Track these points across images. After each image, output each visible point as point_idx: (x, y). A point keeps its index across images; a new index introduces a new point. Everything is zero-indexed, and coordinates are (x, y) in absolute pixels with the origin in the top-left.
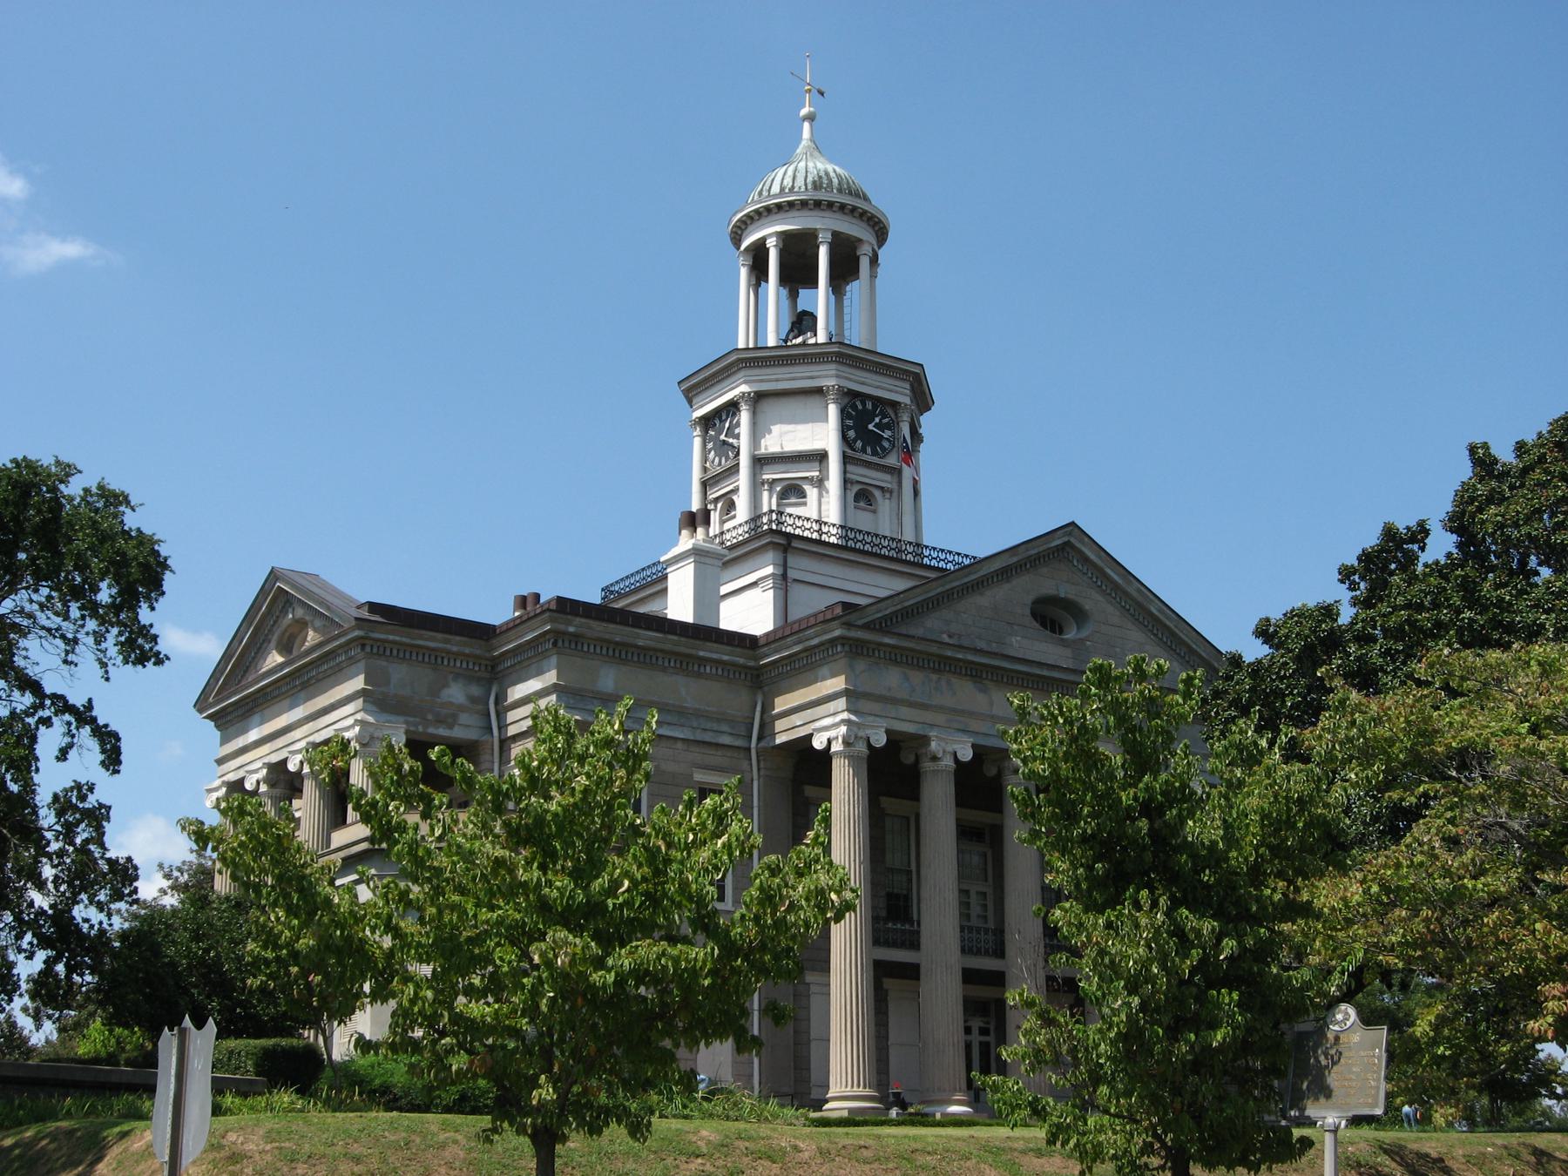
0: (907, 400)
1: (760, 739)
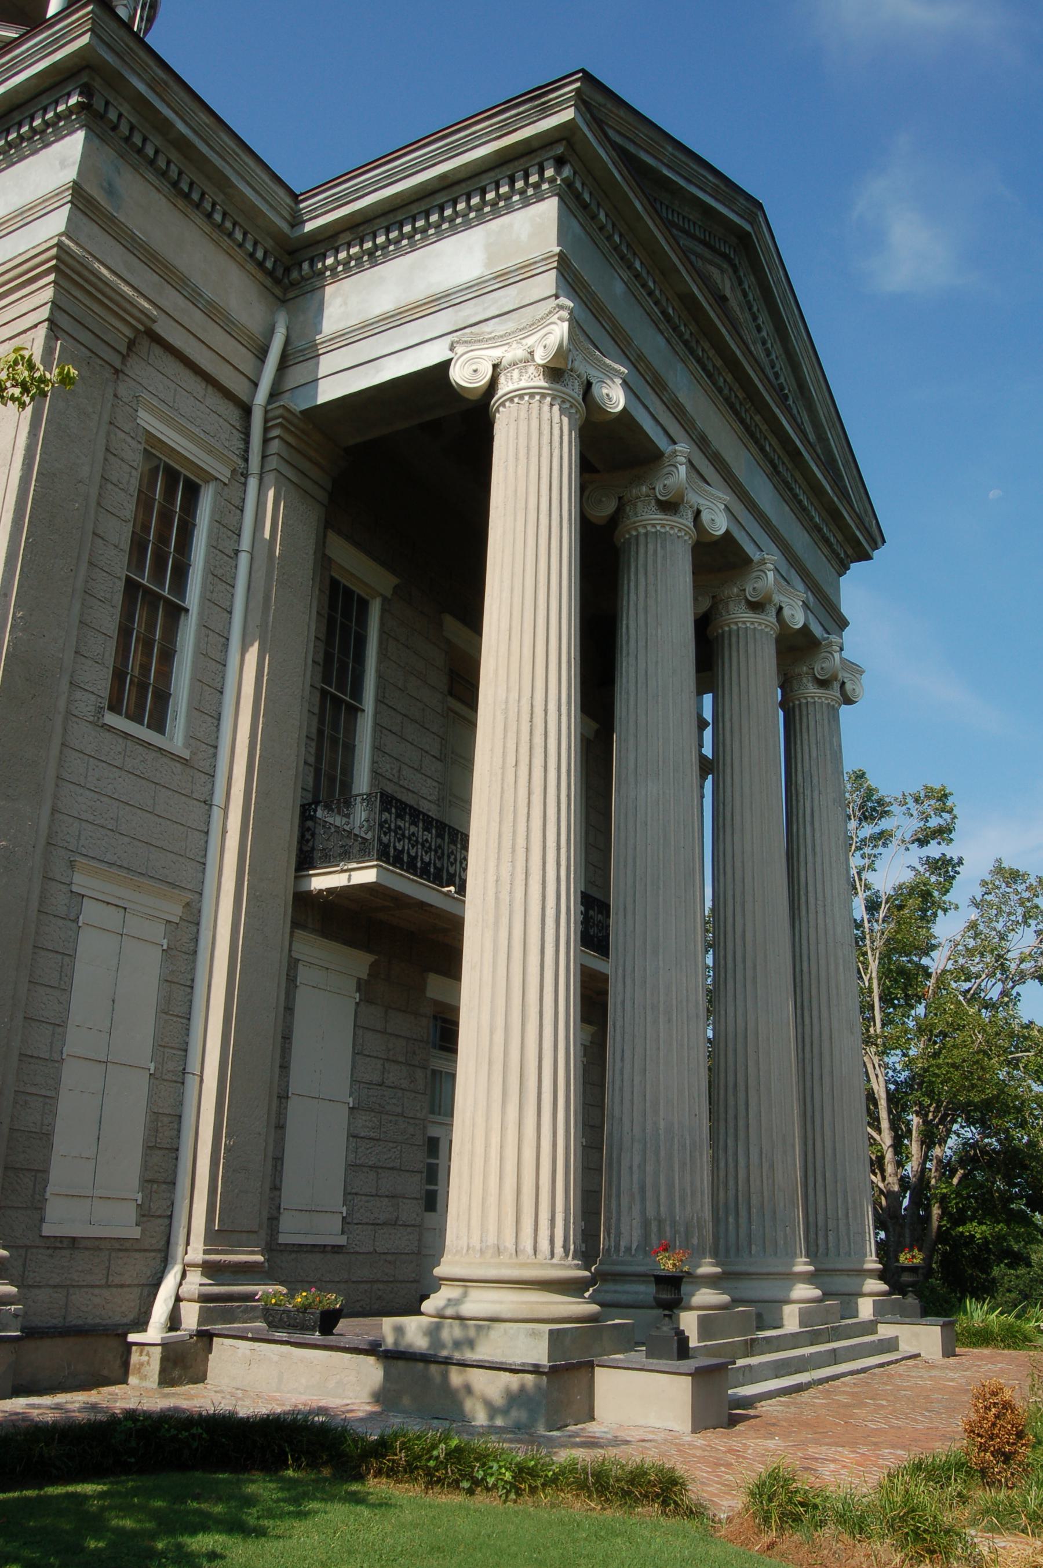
1: (274, 394)
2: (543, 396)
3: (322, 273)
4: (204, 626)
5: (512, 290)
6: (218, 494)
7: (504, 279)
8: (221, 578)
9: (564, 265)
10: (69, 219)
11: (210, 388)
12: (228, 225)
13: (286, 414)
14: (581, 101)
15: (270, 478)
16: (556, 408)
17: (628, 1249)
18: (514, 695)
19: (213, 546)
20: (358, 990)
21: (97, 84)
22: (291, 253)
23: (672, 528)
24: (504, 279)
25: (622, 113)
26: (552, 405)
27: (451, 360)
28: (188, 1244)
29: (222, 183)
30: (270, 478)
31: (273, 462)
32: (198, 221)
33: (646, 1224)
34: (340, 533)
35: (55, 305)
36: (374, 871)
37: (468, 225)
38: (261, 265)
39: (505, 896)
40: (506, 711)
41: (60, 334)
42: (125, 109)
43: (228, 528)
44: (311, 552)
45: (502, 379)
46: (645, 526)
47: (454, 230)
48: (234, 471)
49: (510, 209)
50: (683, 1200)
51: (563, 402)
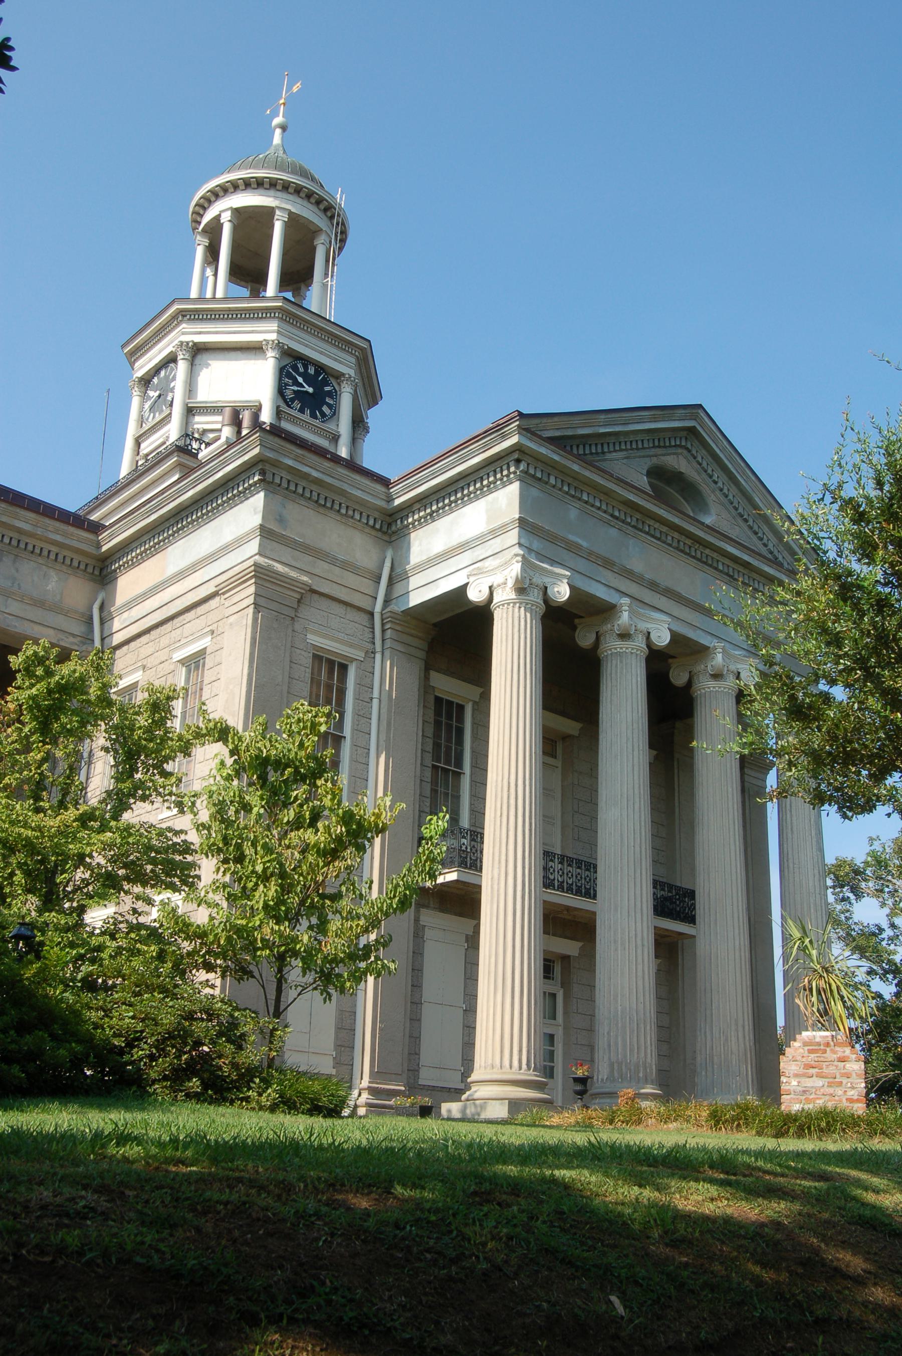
0: (352, 373)
1: (387, 602)
2: (515, 603)
3: (407, 526)
4: (354, 745)
5: (498, 540)
6: (358, 668)
7: (494, 533)
8: (362, 716)
9: (522, 523)
10: (260, 545)
11: (349, 608)
12: (350, 513)
13: (392, 615)
14: (522, 430)
15: (387, 653)
16: (523, 609)
17: (602, 1080)
18: (500, 778)
19: (356, 698)
20: (467, 941)
21: (267, 467)
22: (390, 515)
23: (627, 648)
24: (494, 533)
25: (556, 419)
26: (520, 607)
27: (468, 583)
28: (362, 1079)
29: (343, 493)
30: (387, 653)
31: (388, 643)
32: (333, 516)
33: (611, 1065)
34: (438, 671)
35: (257, 595)
36: (456, 874)
37: (477, 498)
38: (373, 527)
39: (496, 887)
40: (497, 786)
41: (260, 609)
42: (284, 474)
43: (365, 686)
44: (416, 690)
45: (495, 594)
46: (610, 650)
47: (471, 501)
48: (367, 652)
49: (497, 489)
50: (631, 1050)
51: (527, 604)
